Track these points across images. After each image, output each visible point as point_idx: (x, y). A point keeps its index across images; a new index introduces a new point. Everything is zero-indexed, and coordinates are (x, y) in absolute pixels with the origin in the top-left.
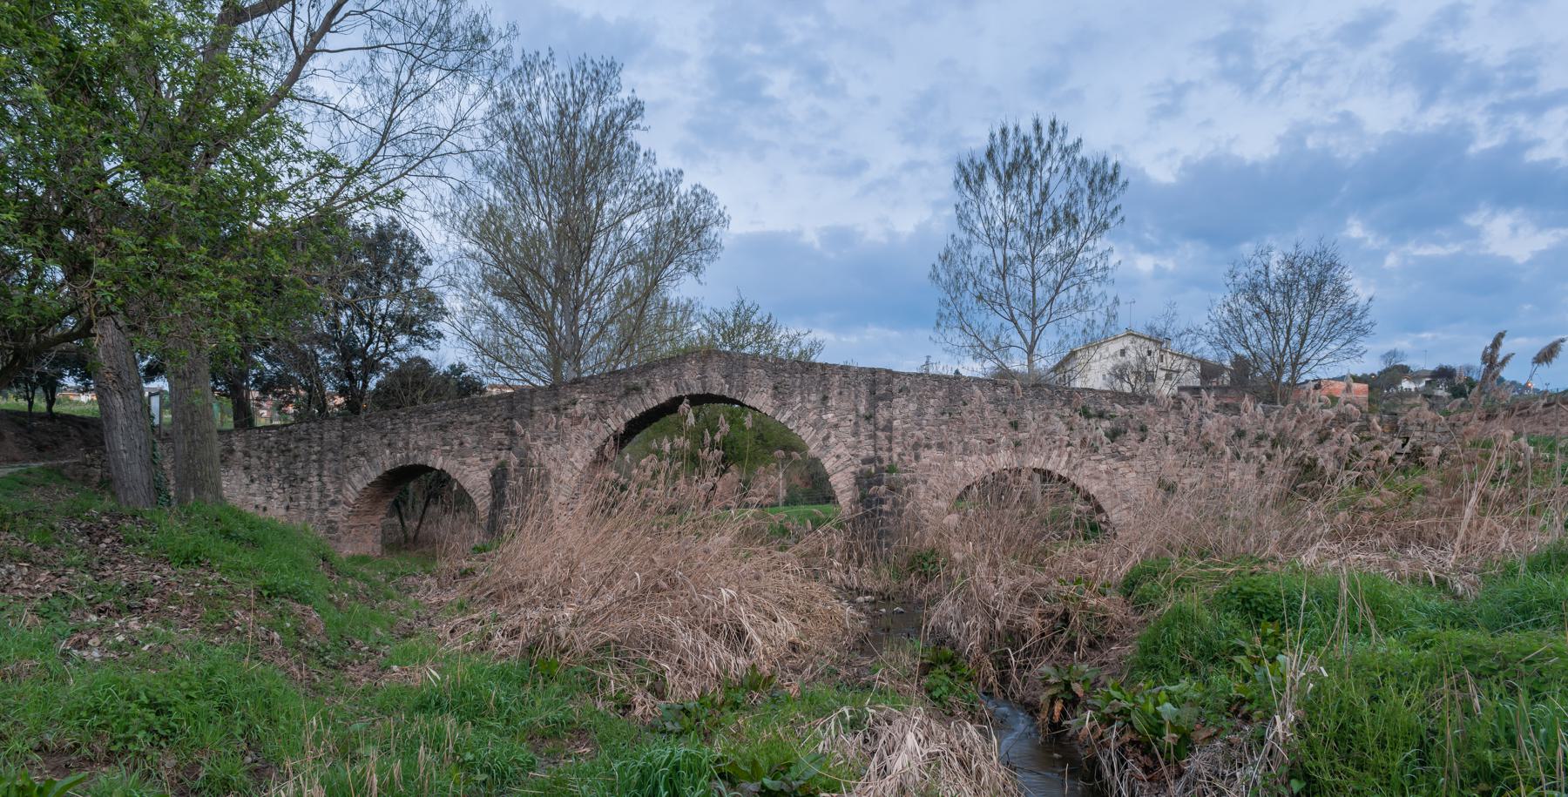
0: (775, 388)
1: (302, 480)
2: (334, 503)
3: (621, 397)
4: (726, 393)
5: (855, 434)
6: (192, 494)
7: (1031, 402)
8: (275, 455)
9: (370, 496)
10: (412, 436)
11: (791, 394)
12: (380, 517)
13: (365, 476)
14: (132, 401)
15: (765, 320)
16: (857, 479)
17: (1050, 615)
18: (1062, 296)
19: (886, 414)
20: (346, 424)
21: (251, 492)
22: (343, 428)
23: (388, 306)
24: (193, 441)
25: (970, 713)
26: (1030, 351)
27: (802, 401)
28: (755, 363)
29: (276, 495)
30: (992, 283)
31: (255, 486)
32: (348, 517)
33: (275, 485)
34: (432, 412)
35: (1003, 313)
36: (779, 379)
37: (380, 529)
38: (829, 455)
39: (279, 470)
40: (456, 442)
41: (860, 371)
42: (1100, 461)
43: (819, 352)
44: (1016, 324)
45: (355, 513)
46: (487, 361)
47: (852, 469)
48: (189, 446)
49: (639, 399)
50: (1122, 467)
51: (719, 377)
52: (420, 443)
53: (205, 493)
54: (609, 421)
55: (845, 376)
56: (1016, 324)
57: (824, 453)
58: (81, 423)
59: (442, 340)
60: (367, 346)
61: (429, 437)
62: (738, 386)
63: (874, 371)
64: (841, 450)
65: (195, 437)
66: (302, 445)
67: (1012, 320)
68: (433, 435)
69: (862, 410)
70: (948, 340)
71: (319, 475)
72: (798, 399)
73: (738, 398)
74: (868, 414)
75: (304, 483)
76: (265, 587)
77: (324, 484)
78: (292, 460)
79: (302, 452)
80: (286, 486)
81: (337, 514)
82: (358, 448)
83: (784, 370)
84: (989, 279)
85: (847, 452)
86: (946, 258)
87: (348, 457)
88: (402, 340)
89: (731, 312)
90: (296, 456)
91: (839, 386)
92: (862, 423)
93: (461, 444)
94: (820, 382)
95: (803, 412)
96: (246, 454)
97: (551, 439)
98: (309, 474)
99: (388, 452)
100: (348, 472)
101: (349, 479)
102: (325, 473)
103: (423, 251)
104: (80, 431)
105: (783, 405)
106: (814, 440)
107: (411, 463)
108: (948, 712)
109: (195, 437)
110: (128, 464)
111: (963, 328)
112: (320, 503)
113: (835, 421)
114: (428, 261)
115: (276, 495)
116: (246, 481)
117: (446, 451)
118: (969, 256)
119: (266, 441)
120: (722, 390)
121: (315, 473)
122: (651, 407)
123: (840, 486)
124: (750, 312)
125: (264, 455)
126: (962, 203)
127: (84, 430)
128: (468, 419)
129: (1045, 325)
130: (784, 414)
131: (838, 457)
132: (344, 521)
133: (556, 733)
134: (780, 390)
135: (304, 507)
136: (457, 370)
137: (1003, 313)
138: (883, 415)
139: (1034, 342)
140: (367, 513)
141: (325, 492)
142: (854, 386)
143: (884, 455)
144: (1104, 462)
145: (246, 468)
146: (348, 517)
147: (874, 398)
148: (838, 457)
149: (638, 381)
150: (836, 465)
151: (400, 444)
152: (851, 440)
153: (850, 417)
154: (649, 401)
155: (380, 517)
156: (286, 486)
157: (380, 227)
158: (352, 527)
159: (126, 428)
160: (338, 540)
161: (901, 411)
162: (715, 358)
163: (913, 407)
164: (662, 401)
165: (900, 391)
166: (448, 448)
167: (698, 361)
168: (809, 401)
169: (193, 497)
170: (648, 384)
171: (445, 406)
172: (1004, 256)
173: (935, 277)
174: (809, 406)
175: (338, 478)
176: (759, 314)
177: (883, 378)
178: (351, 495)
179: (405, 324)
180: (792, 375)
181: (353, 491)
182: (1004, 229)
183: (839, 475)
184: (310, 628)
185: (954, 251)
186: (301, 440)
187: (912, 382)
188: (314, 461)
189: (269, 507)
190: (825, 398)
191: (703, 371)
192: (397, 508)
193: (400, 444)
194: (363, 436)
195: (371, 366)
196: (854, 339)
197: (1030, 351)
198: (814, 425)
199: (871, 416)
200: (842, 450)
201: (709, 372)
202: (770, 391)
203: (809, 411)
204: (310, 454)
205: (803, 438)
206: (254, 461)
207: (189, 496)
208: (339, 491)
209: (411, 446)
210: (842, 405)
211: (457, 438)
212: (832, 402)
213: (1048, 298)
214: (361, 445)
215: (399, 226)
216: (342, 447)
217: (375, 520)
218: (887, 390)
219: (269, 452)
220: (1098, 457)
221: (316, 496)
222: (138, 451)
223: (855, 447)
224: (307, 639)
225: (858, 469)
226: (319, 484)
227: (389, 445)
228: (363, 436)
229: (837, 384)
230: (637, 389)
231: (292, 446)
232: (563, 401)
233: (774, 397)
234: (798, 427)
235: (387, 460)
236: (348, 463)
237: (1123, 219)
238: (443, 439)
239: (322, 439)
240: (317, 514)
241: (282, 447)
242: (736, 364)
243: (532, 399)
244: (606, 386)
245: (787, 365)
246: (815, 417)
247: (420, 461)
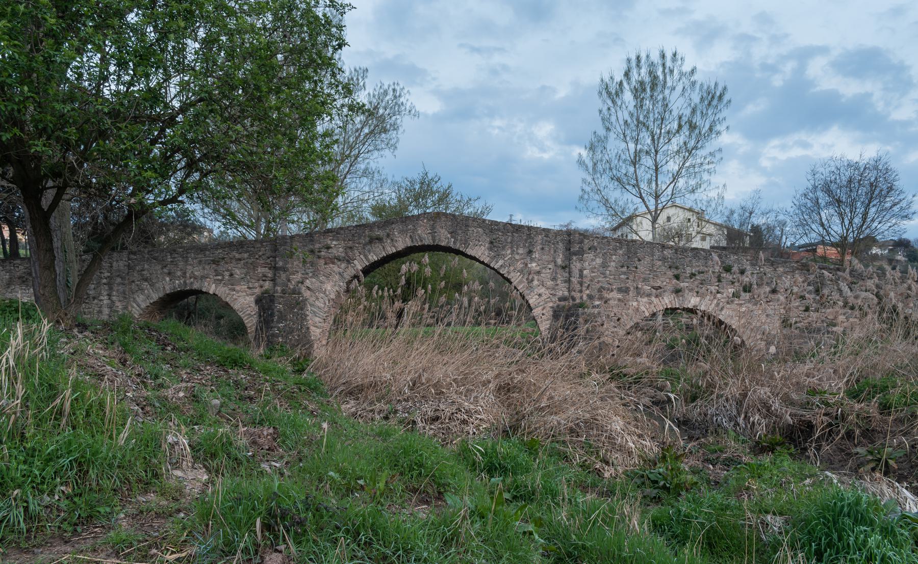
1: (94, 298)
40: (227, 273)
61: (204, 268)
68: (207, 267)
77: (113, 302)
98: (100, 294)
102: (114, 293)
121: (105, 293)
128: (237, 256)
141: (114, 308)
188: (105, 284)
193: (179, 273)
194: (146, 266)
204: (101, 278)
209: (188, 275)
214: (145, 273)
226: (109, 301)
228: (146, 266)
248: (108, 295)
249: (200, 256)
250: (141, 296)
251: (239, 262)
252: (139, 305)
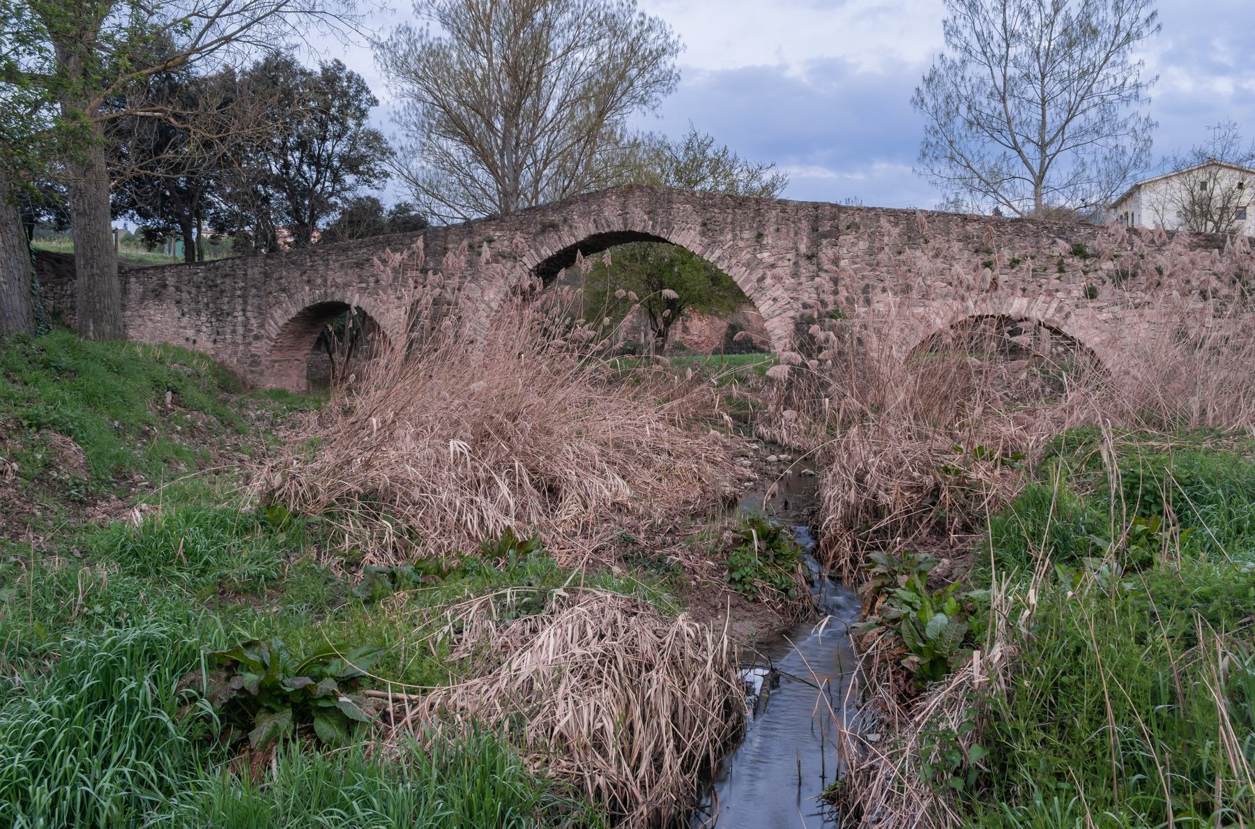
0: (704, 225)
1: (228, 314)
2: (257, 338)
3: (536, 235)
4: (649, 230)
5: (795, 275)
6: (91, 325)
7: (1010, 240)
9: (291, 332)
10: (330, 273)
11: (722, 232)
12: (305, 352)
13: (286, 312)
14: (10, 235)
15: (721, 154)
16: (797, 325)
17: (919, 489)
18: (1078, 120)
19: (830, 252)
20: (269, 261)
21: (182, 325)
22: (266, 265)
23: (333, 147)
24: (93, 275)
25: (782, 600)
26: (1039, 180)
27: (734, 239)
28: (682, 198)
29: (204, 329)
30: (989, 106)
31: (185, 320)
32: (271, 351)
33: (204, 319)
34: (348, 249)
35: (1003, 140)
36: (708, 215)
37: (305, 365)
38: (764, 298)
39: (207, 305)
40: (372, 279)
41: (800, 206)
42: (1100, 309)
43: (783, 188)
44: (1020, 152)
45: (277, 347)
46: (423, 200)
47: (792, 313)
48: (89, 280)
49: (556, 237)
50: (1131, 316)
51: (642, 213)
52: (338, 280)
53: (103, 324)
54: (525, 259)
55: (784, 211)
56: (1020, 152)
57: (758, 295)
58: (55, 259)
59: (388, 179)
60: (315, 185)
61: (346, 274)
62: (662, 223)
63: (816, 206)
64: (779, 292)
65: (95, 271)
66: (228, 281)
67: (1016, 147)
68: (350, 272)
69: (803, 248)
70: (936, 172)
71: (244, 310)
72: (729, 236)
73: (662, 236)
74: (809, 253)
75: (230, 318)
76: (27, 418)
77: (247, 319)
78: (218, 295)
79: (228, 288)
80: (213, 320)
81: (260, 348)
83: (714, 206)
84: (985, 102)
85: (786, 295)
86: (931, 80)
87: (271, 293)
88: (349, 179)
89: (683, 146)
90: (222, 292)
91: (777, 223)
92: (803, 262)
93: (377, 281)
94: (754, 218)
95: (735, 250)
96: (178, 289)
97: (465, 277)
98: (234, 309)
99: (307, 288)
100: (271, 307)
101: (272, 314)
102: (249, 308)
103: (368, 92)
104: (53, 266)
105: (712, 244)
106: (747, 281)
107: (329, 300)
108: (750, 598)
109: (95, 271)
110: (8, 296)
111: (952, 158)
112: (244, 337)
113: (771, 260)
114: (374, 102)
115: (204, 329)
116: (178, 314)
117: (362, 288)
118: (963, 78)
119: (195, 277)
120: (645, 227)
121: (239, 308)
122: (569, 244)
123: (777, 332)
124: (703, 147)
125: (194, 290)
126: (951, 17)
127: (56, 265)
129: (1055, 155)
130: (712, 253)
131: (775, 300)
132: (266, 356)
133: (254, 590)
134: (709, 226)
135: (229, 341)
136: (402, 209)
137: (1003, 140)
138: (826, 253)
139: (1043, 171)
140: (290, 348)
142: (794, 222)
143: (830, 299)
144: (1105, 310)
145: (178, 302)
146: (271, 351)
147: (817, 236)
148: (775, 300)
149: (555, 217)
150: (773, 308)
151: (319, 281)
152: (789, 282)
153: (789, 256)
154: (566, 239)
155: (304, 352)
157: (325, 70)
158: (276, 361)
159: (5, 261)
160: (261, 374)
161: (851, 248)
162: (638, 193)
163: (863, 245)
164: (581, 238)
165: (848, 228)
166: (364, 285)
167: (619, 197)
168: (742, 239)
169: (92, 328)
170: (565, 221)
171: (361, 243)
172: (1004, 76)
173: (919, 102)
174: (741, 244)
175: (261, 314)
176: (714, 146)
177: (827, 213)
178: (273, 330)
179: (351, 163)
180: (722, 211)
182: (1004, 45)
183: (776, 319)
184: (65, 461)
185: (942, 71)
186: (226, 276)
187: (862, 218)
188: (239, 297)
189: (198, 340)
190: (760, 236)
191: (624, 207)
192: (323, 343)
193: (319, 281)
194: (284, 273)
195: (322, 206)
196: (859, 177)
197: (1039, 180)
198: (747, 265)
199: (813, 256)
200: (779, 293)
201: (631, 208)
202: (698, 228)
203: (741, 249)
205: (735, 279)
206: (185, 296)
207: (89, 327)
208: (261, 326)
210: (780, 243)
211: (373, 276)
212: (768, 240)
213: (1058, 123)
214: (283, 281)
215: (344, 68)
216: (264, 283)
217: (300, 355)
218: (831, 226)
219: (198, 287)
220: (1099, 304)
221: (240, 330)
222: (17, 283)
223: (795, 290)
224: (58, 471)
225: (798, 315)
226: (243, 318)
227: (309, 282)
228: (284, 273)
229: (774, 220)
230: (554, 226)
232: (477, 238)
233: (703, 234)
234: (729, 267)
235: (307, 297)
236: (271, 299)
237: (1159, 26)
238: (360, 276)
239: (245, 275)
240: (241, 348)
241: (210, 283)
242: (659, 199)
243: (446, 237)
244: (521, 223)
245: (717, 200)
246: (748, 256)
247: (337, 298)
249: (342, 258)
250: (279, 311)
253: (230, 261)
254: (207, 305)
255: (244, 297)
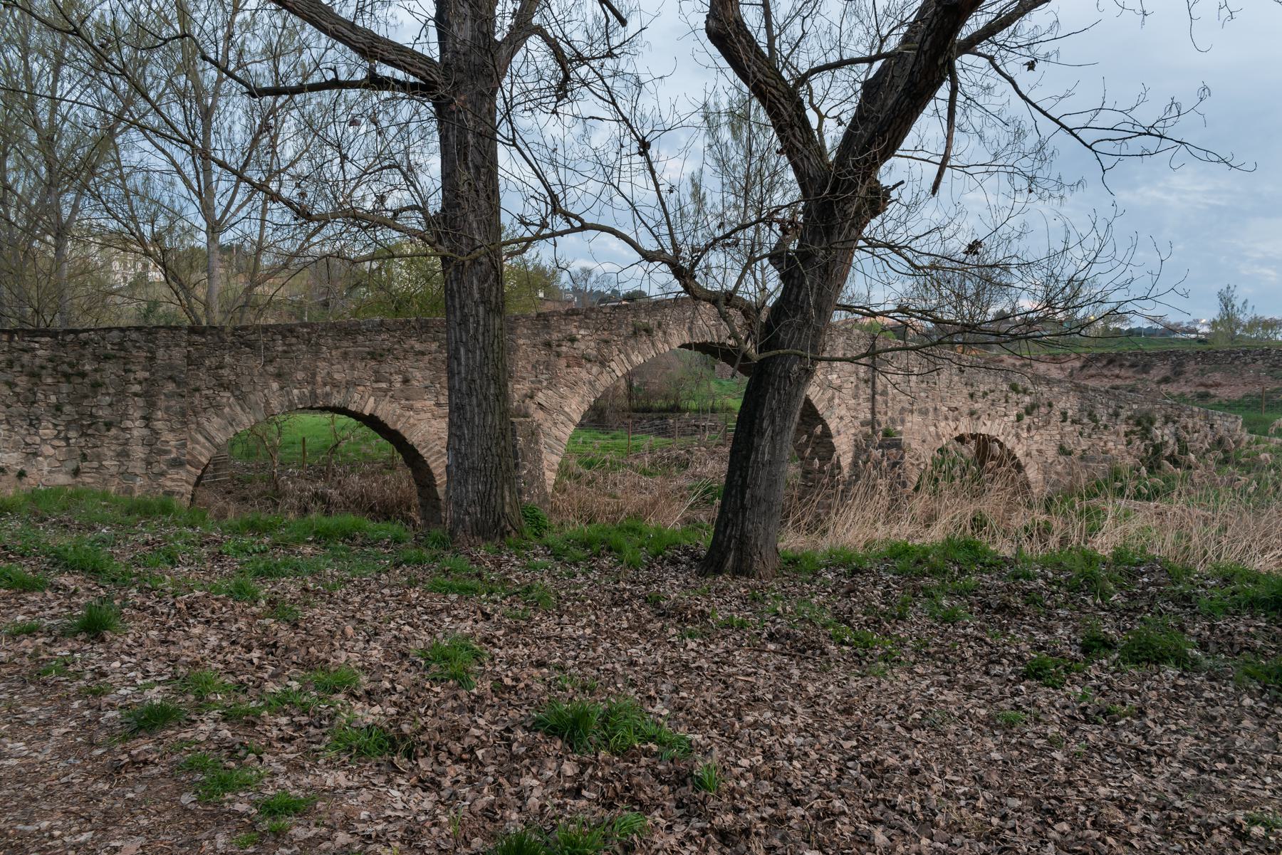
1: (109, 425)
8: (49, 380)
21: (156, 470)
39: (58, 408)
52: (336, 376)
61: (353, 368)
66: (111, 369)
68: (359, 365)
77: (155, 433)
82: (218, 377)
90: (96, 386)
98: (125, 416)
112: (149, 464)
121: (137, 414)
128: (418, 346)
141: (159, 445)
156: (72, 434)
181: (207, 444)
188: (136, 395)
194: (228, 359)
204: (128, 382)
209: (319, 379)
214: (225, 372)
221: (139, 452)
226: (146, 432)
228: (228, 359)
231: (87, 367)
238: (376, 372)
239: (152, 359)
241: (65, 368)
248: (143, 418)
249: (345, 344)
250: (215, 419)
251: (419, 357)
252: (209, 438)
253: (115, 333)
254: (58, 408)
255: (149, 398)
